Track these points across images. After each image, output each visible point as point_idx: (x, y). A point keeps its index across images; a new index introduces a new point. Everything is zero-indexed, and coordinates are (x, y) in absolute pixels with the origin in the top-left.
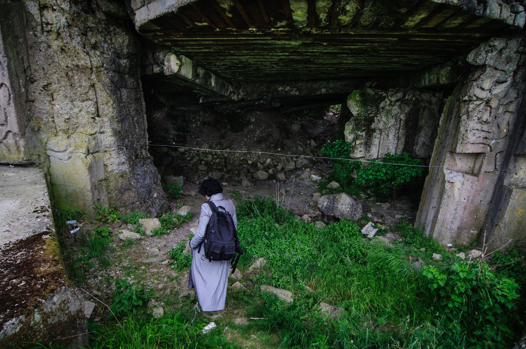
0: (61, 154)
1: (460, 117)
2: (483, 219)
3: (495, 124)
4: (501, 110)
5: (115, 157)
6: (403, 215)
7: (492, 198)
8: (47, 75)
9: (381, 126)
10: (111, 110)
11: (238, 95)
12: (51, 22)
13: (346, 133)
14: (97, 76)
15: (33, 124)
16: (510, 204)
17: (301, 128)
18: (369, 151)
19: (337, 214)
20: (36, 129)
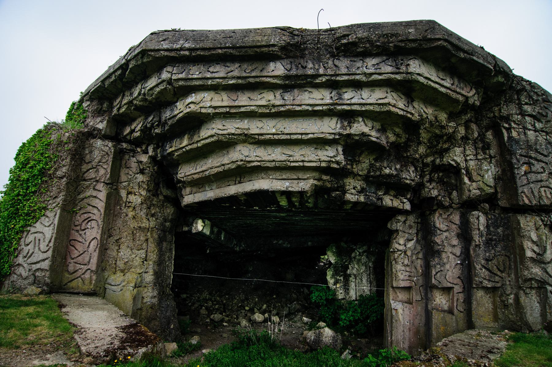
4: (414, 258)
9: (354, 271)
10: (155, 256)
11: (240, 247)
13: (328, 278)
14: (151, 234)
16: (434, 323)
18: (348, 293)
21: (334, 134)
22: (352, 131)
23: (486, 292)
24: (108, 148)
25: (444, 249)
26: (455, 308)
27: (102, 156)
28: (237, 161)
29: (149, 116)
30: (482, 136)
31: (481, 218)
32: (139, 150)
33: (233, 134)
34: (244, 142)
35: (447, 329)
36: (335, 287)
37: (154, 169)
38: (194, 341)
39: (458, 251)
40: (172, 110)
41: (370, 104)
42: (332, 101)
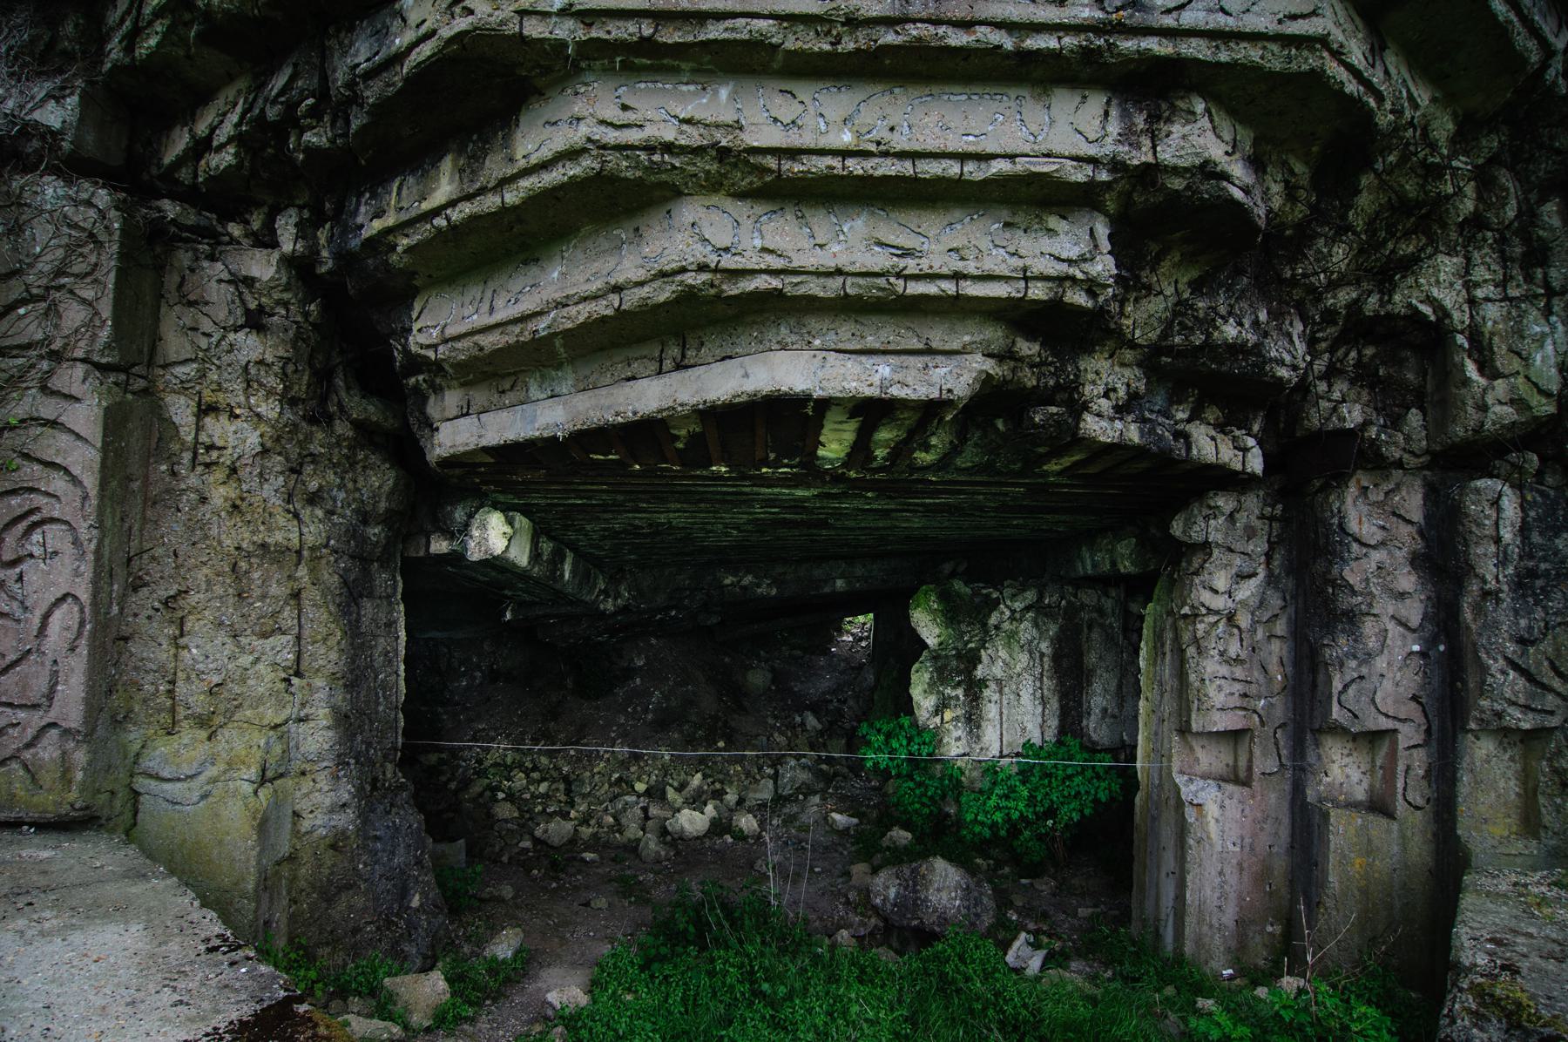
0: (179, 785)
1: (1183, 651)
2: (1284, 891)
3: (1256, 666)
4: (1260, 634)
5: (326, 788)
6: (1096, 906)
7: (1293, 835)
8: (182, 571)
9: (997, 671)
10: (334, 656)
11: (615, 599)
12: (220, 443)
13: (916, 692)
14: (312, 571)
15: (116, 700)
16: (1332, 846)
17: (773, 681)
18: (978, 737)
19: (930, 920)
20: (120, 717)
21: (1093, 161)
22: (1167, 154)
23: (1501, 743)
24: (92, 213)
25: (1370, 605)
26: (1400, 797)
27: (71, 249)
28: (683, 270)
29: (272, 71)
30: (1528, 215)
31: (1505, 502)
32: (235, 230)
33: (668, 148)
34: (713, 185)
35: (1370, 865)
36: (938, 720)
37: (306, 315)
38: (504, 947)
39: (1414, 612)
40: (382, 34)
41: (1255, 37)
42: (1100, 15)
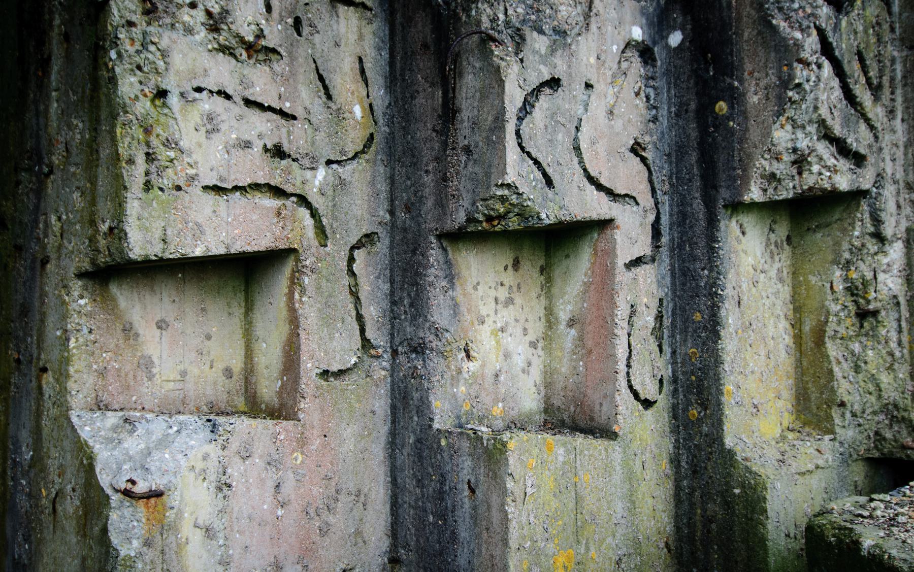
7: (395, 531)
